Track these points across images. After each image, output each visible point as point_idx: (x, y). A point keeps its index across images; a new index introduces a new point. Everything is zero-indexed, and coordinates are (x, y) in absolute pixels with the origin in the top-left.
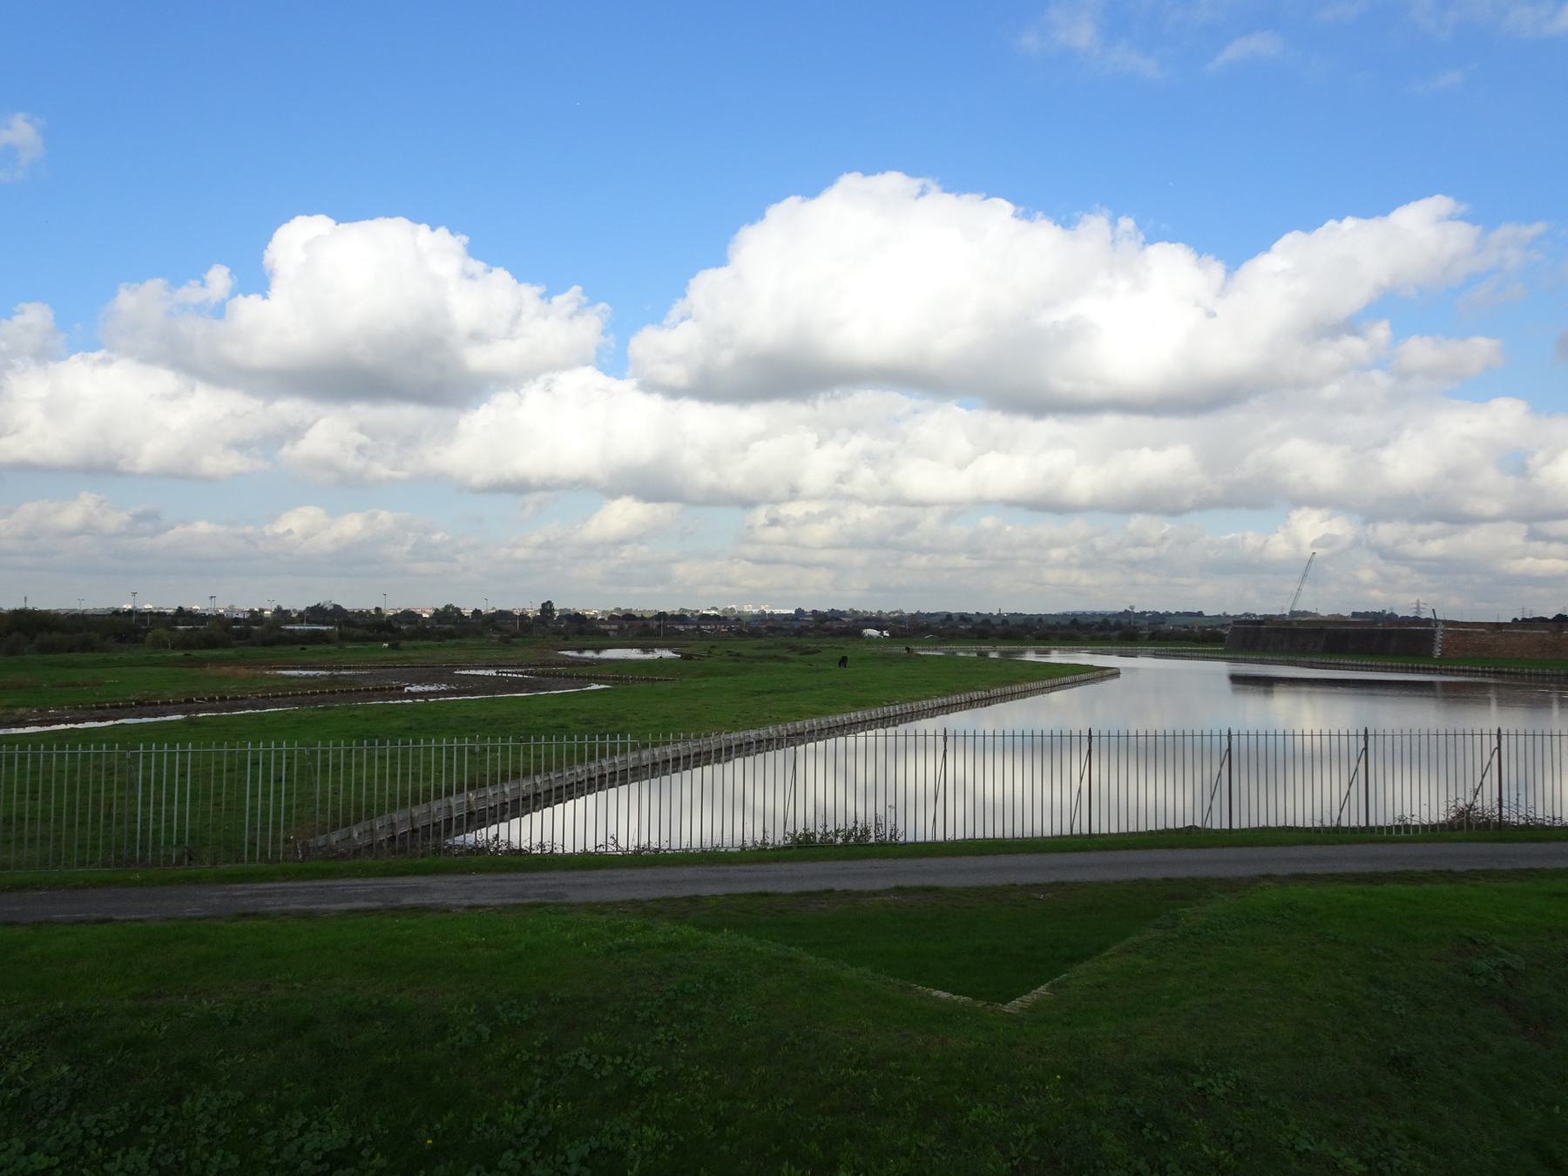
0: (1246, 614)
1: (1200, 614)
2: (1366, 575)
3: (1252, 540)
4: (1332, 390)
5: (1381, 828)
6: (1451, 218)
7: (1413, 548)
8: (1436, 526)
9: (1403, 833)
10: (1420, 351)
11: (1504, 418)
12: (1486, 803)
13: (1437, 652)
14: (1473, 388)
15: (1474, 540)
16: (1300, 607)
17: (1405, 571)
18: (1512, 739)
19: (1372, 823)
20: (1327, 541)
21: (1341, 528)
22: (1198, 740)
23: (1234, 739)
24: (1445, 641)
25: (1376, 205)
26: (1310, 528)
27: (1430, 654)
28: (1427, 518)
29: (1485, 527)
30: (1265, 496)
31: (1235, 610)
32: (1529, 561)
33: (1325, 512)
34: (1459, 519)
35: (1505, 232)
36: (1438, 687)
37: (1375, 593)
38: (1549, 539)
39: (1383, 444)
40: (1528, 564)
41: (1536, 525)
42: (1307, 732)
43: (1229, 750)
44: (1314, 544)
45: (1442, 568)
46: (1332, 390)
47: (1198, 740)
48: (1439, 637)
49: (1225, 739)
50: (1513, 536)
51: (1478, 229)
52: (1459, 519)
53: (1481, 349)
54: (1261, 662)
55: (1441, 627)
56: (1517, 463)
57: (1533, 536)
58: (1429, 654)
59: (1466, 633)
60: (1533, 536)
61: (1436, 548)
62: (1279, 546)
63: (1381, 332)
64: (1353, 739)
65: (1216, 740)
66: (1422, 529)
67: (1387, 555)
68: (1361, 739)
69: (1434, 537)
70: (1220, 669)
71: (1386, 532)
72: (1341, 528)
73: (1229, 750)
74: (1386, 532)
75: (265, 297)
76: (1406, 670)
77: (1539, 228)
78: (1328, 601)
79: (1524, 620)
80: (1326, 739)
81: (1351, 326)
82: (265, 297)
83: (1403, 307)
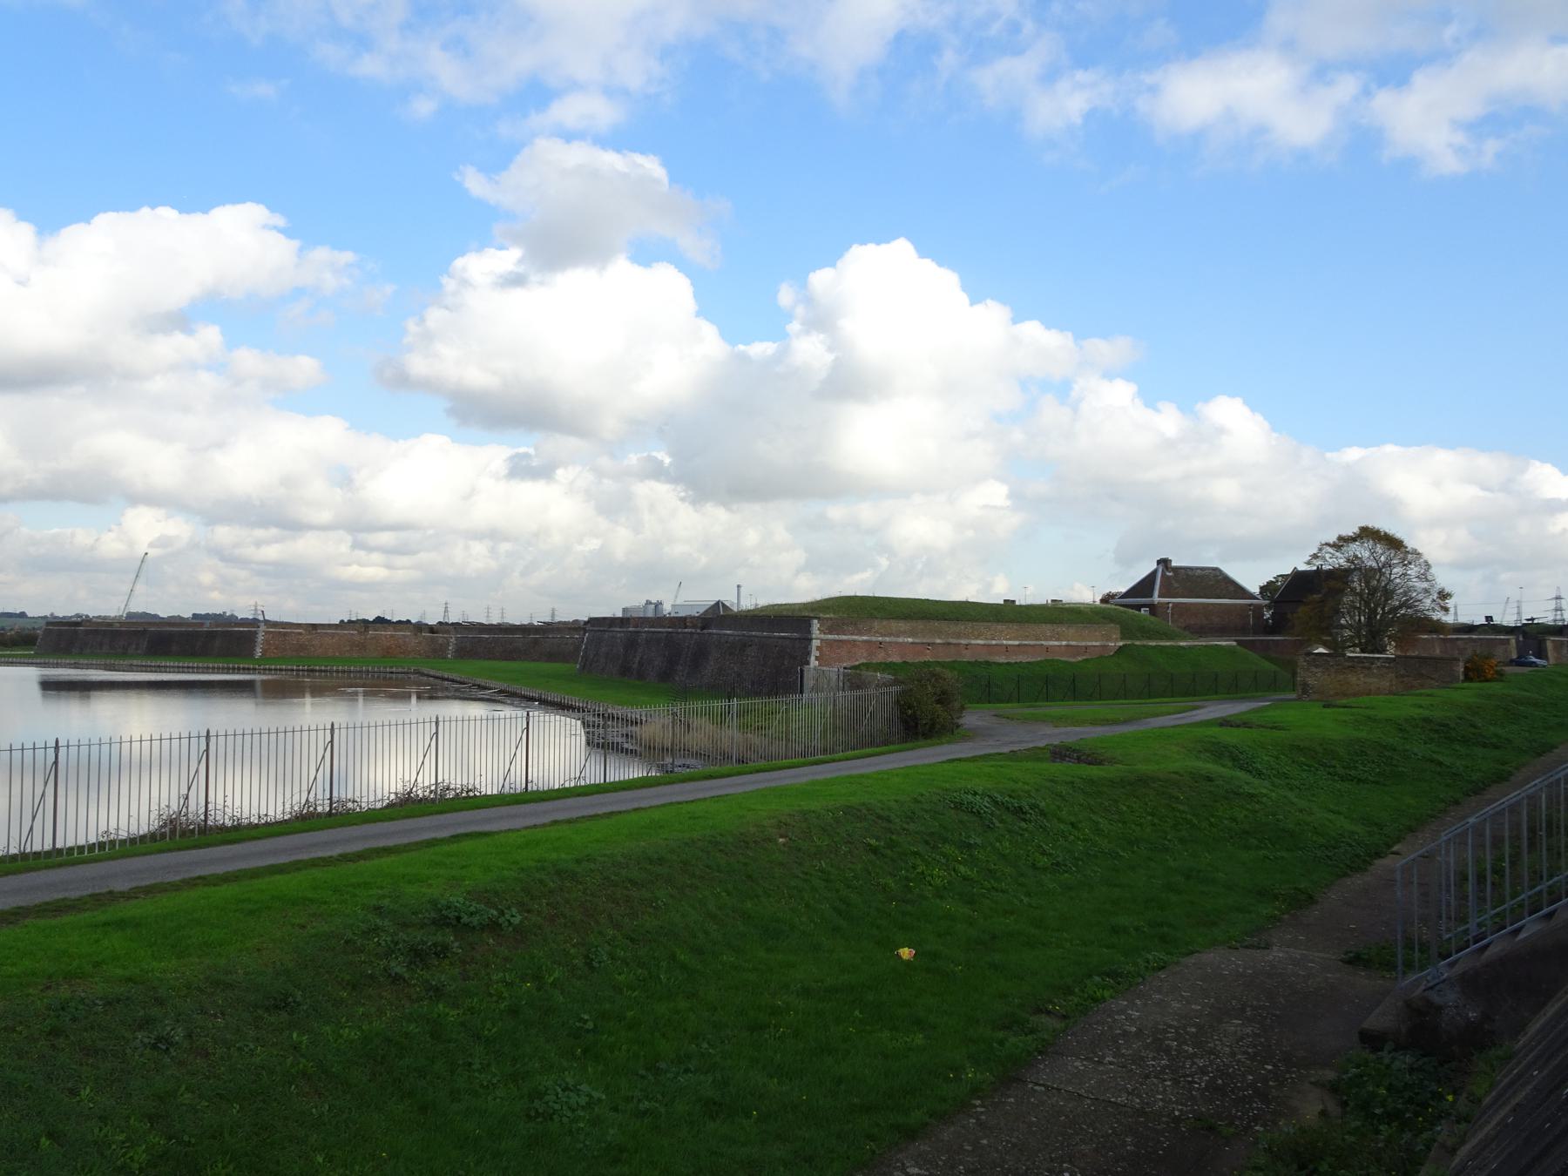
0: (78, 616)
1: (23, 615)
2: (207, 578)
3: (82, 537)
4: (158, 385)
5: (71, 849)
6: (265, 227)
7: (249, 552)
8: (274, 531)
9: (240, 833)
10: (248, 360)
11: (326, 435)
12: (195, 807)
13: (258, 652)
14: (291, 400)
15: (307, 547)
16: (138, 606)
17: (243, 574)
18: (344, 731)
19: (58, 846)
20: (163, 542)
21: (178, 528)
22: (28, 754)
23: (62, 751)
24: (266, 642)
25: (195, 201)
26: (145, 529)
27: (251, 654)
28: (264, 523)
29: (310, 535)
30: (95, 490)
31: (64, 610)
32: (354, 569)
33: (161, 512)
34: (294, 527)
35: (322, 254)
36: (259, 688)
37: (215, 595)
38: (370, 549)
39: (220, 445)
40: (353, 572)
41: (362, 536)
42: (136, 737)
43: (56, 762)
44: (151, 545)
45: (280, 571)
46: (158, 385)
47: (28, 754)
48: (260, 638)
49: (51, 752)
50: (340, 545)
51: (295, 244)
52: (294, 527)
53: (305, 367)
54: (76, 666)
55: (263, 628)
56: (344, 479)
57: (357, 545)
58: (250, 654)
59: (285, 634)
60: (357, 545)
61: (272, 552)
62: (111, 546)
63: (211, 335)
64: (321, 733)
65: (40, 753)
66: (260, 533)
67: (224, 556)
68: (203, 740)
69: (268, 542)
70: (27, 676)
71: (224, 534)
72: (178, 528)
73: (56, 762)
74: (224, 534)
75: (972, 304)
76: (227, 670)
77: (348, 257)
78: (169, 601)
79: (350, 622)
80: (156, 744)
81: (181, 320)
82: (972, 304)
83: (235, 313)
